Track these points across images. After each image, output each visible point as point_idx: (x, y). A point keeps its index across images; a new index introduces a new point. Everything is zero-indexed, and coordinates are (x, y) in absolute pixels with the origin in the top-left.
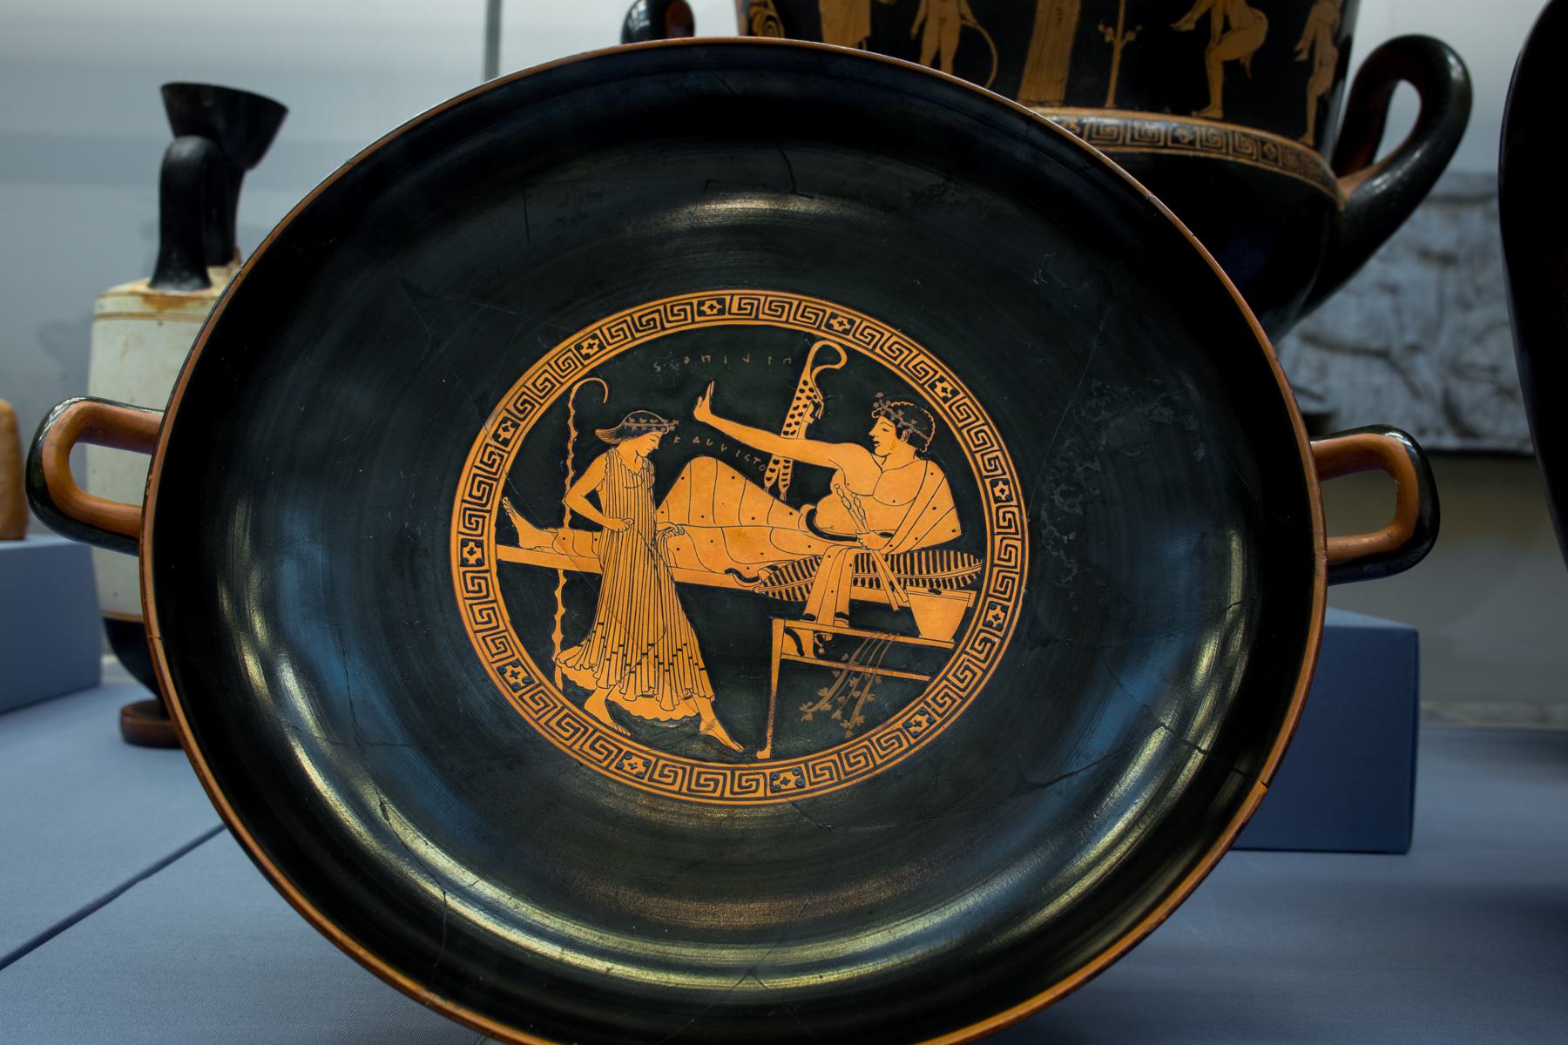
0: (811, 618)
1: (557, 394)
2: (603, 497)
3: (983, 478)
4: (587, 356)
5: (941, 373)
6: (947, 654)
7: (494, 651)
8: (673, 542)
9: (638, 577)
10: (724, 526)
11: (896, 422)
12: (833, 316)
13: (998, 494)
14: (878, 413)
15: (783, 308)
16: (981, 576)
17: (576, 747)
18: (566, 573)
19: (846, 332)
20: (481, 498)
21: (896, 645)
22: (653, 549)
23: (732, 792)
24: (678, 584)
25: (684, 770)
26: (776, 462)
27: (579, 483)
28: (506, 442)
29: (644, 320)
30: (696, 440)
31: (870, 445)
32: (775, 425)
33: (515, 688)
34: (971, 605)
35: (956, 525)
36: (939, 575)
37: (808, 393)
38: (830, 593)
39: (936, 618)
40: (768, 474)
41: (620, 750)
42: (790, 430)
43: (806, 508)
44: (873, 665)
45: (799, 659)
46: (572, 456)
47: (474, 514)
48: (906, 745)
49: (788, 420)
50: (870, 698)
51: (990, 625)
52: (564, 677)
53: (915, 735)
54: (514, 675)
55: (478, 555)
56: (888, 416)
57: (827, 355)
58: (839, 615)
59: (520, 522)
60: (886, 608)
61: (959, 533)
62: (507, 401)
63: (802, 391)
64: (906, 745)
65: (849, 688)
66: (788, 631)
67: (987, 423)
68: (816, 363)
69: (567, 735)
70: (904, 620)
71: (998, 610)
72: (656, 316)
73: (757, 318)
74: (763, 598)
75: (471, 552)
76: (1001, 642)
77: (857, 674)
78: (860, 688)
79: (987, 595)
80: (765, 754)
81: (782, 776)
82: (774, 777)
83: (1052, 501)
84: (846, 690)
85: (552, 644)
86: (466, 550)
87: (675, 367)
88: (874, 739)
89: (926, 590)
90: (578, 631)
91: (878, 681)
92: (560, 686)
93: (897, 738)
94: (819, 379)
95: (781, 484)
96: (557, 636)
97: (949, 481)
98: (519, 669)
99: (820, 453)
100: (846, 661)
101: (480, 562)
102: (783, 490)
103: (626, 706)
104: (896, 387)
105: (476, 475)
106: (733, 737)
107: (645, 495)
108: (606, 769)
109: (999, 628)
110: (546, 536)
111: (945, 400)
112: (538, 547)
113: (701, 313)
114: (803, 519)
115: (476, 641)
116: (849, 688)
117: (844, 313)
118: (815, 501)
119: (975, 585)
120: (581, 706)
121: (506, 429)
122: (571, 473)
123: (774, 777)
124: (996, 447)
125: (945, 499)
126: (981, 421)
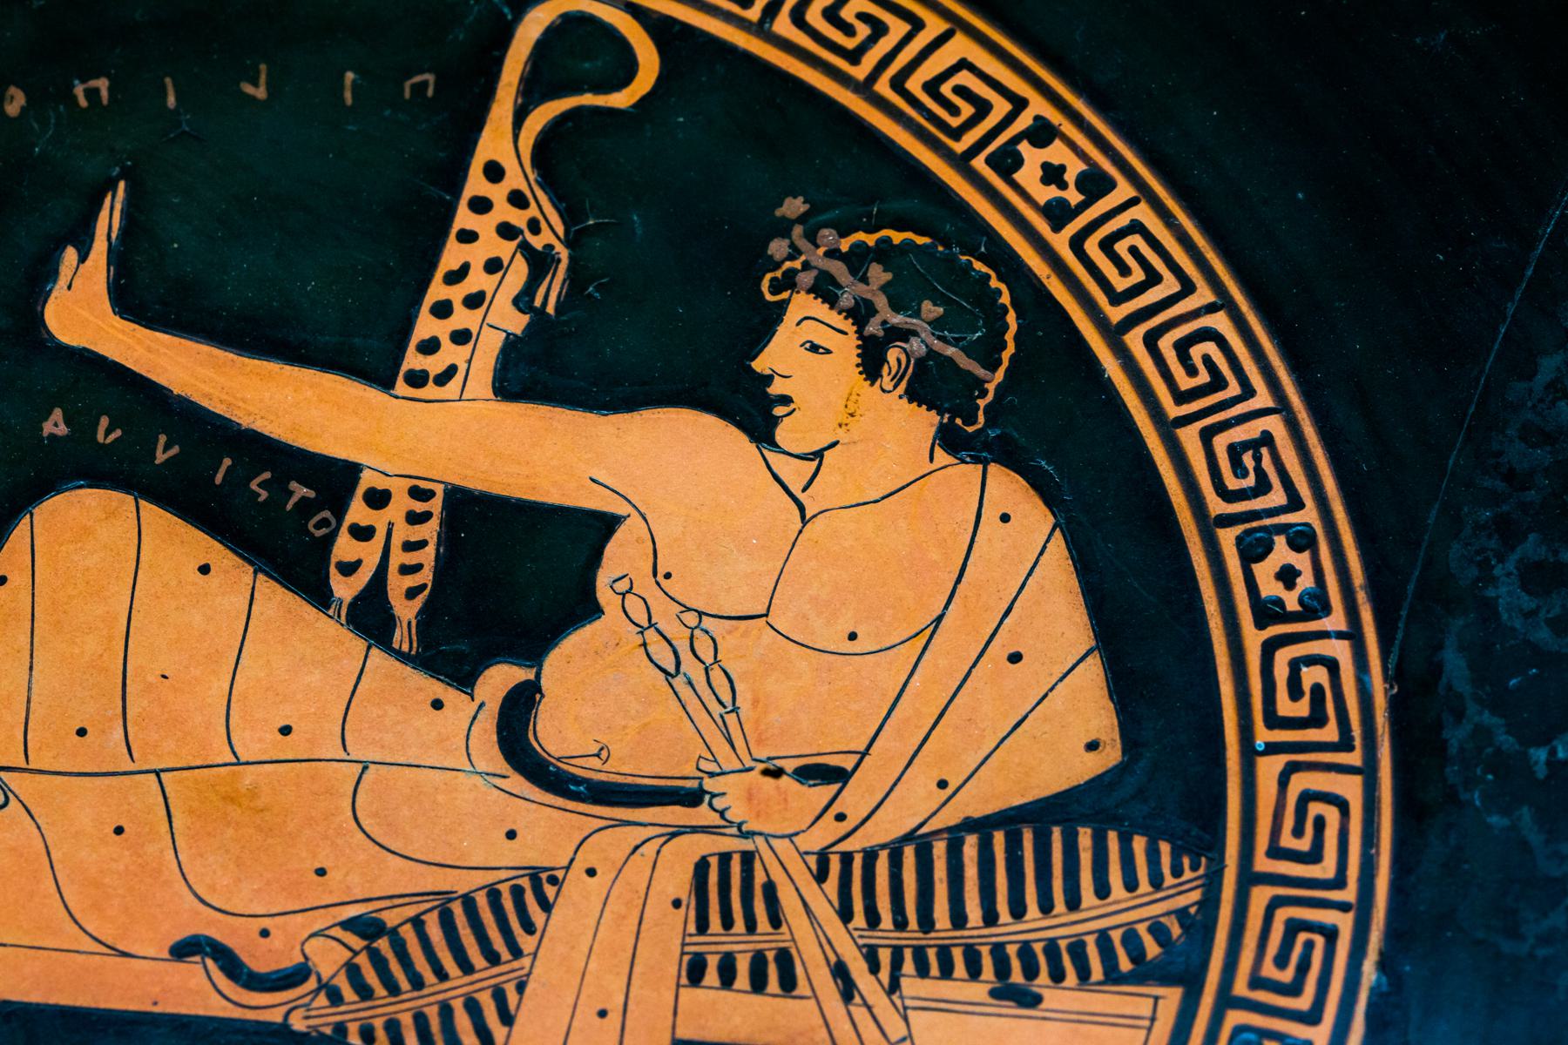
3: (1209, 526)
5: (1038, 106)
11: (860, 313)
13: (1270, 589)
14: (788, 282)
26: (378, 499)
31: (755, 412)
32: (374, 357)
35: (1101, 719)
40: (345, 547)
43: (500, 679)
49: (427, 325)
56: (825, 290)
63: (481, 205)
67: (1224, 303)
68: (533, 91)
79: (1226, 1000)
83: (1488, 609)
95: (397, 585)
97: (1073, 545)
102: (406, 611)
111: (1058, 214)
118: (533, 648)
124: (1263, 399)
125: (1058, 619)
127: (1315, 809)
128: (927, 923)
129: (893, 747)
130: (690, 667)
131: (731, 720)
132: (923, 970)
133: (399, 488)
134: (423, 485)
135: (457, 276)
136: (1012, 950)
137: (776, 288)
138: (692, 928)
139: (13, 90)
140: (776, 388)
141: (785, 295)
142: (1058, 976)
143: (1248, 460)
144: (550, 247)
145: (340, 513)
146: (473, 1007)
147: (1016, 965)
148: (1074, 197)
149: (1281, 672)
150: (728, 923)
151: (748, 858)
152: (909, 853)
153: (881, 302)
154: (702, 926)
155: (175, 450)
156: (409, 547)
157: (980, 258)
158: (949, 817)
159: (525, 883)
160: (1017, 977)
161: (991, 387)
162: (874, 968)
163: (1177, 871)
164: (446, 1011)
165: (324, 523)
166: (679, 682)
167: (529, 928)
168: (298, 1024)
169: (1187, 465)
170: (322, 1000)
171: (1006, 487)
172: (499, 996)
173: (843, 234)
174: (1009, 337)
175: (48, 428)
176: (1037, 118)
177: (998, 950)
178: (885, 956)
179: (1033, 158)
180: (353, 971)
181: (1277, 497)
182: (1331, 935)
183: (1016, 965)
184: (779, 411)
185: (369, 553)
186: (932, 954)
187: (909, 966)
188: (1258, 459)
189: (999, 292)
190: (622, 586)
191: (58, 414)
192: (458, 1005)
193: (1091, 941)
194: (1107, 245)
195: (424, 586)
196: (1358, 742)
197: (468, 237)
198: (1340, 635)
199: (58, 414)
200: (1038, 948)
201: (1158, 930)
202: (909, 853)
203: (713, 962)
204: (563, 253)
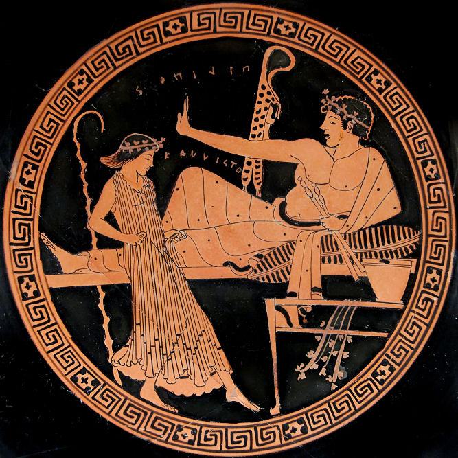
0: (293, 295)
3: (415, 160)
4: (80, 92)
5: (375, 66)
6: (399, 313)
9: (158, 281)
10: (217, 226)
11: (342, 115)
13: (428, 173)
14: (326, 109)
15: (236, 18)
17: (142, 429)
18: (104, 288)
19: (292, 35)
20: (23, 239)
22: (166, 257)
24: (189, 281)
25: (221, 432)
27: (96, 208)
28: (31, 184)
29: (120, 48)
31: (322, 138)
32: (242, 129)
33: (87, 391)
34: (413, 271)
35: (397, 203)
39: (388, 284)
40: (244, 175)
41: (173, 425)
42: (256, 132)
43: (278, 201)
44: (344, 328)
46: (86, 185)
47: (22, 255)
48: (376, 391)
49: (254, 124)
50: (346, 356)
52: (121, 374)
53: (382, 382)
54: (84, 381)
55: (33, 288)
58: (314, 289)
59: (59, 253)
60: (349, 279)
61: (399, 210)
62: (23, 147)
63: (262, 95)
64: (376, 391)
65: (329, 349)
66: (278, 308)
68: (271, 67)
69: (133, 421)
70: (363, 289)
71: (434, 274)
72: (130, 42)
73: (215, 31)
74: (254, 284)
75: (28, 287)
76: (438, 301)
77: (333, 337)
78: (337, 348)
79: (425, 262)
80: (275, 410)
81: (291, 426)
82: (285, 427)
84: (327, 351)
85: (105, 348)
86: (23, 285)
88: (352, 389)
89: (377, 261)
91: (350, 341)
92: (120, 382)
93: (369, 386)
95: (255, 182)
96: (108, 342)
97: (389, 164)
99: (283, 151)
100: (324, 328)
101: (36, 294)
102: (258, 188)
104: (340, 85)
105: (14, 220)
107: (151, 209)
109: (436, 288)
110: (82, 257)
112: (82, 270)
113: (168, 34)
114: (277, 210)
115: (49, 360)
116: (329, 349)
117: (288, 17)
118: (284, 194)
119: (416, 254)
122: (89, 201)
123: (285, 427)
124: (425, 131)
125: (387, 181)
128: (366, 247)
130: (315, 195)
135: (258, 112)
136: (383, 252)
137: (324, 110)
138: (322, 251)
140: (325, 133)
142: (392, 257)
143: (422, 145)
146: (282, 272)
147: (384, 255)
149: (431, 191)
151: (331, 236)
154: (324, 251)
156: (257, 174)
157: (366, 102)
158: (369, 224)
160: (385, 258)
161: (369, 130)
162: (357, 257)
163: (414, 234)
164: (277, 273)
165: (239, 170)
166: (313, 199)
168: (250, 278)
169: (410, 147)
170: (254, 272)
171: (374, 152)
172: (287, 269)
177: (381, 252)
178: (359, 254)
179: (375, 78)
180: (259, 266)
181: (428, 153)
183: (384, 255)
185: (249, 176)
186: (368, 254)
187: (364, 256)
190: (300, 179)
196: (447, 206)
197: (260, 103)
198: (443, 183)
201: (411, 247)
203: (326, 258)
204: (280, 105)
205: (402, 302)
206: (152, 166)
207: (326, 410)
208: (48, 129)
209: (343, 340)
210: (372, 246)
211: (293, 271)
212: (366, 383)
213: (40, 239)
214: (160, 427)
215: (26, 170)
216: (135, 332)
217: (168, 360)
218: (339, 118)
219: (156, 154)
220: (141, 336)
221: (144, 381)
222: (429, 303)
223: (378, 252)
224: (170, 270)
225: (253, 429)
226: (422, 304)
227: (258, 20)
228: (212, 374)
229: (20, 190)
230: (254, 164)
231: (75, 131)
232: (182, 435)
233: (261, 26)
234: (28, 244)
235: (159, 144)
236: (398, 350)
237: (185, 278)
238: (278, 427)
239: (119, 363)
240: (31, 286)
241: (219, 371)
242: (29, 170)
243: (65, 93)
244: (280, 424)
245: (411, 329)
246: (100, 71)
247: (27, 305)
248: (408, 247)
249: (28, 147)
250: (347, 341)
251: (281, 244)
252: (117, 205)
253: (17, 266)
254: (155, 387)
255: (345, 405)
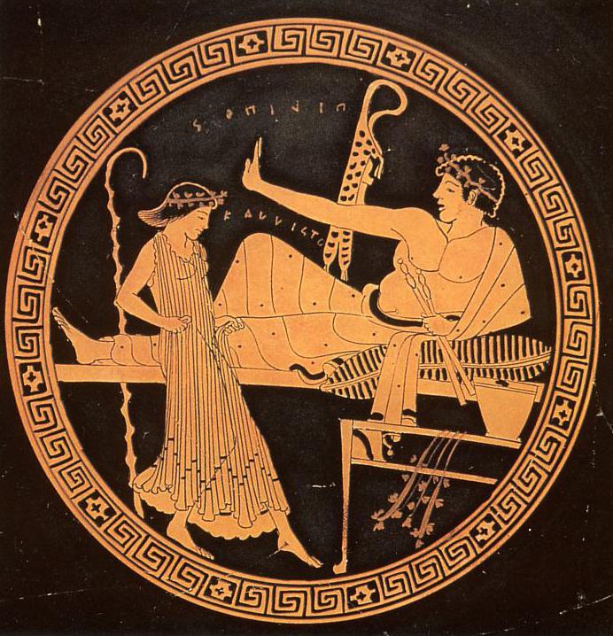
0: (379, 417)
1: (92, 175)
2: (155, 292)
4: (118, 122)
5: (512, 120)
7: (73, 485)
8: (233, 340)
9: (202, 382)
10: (282, 315)
11: (463, 180)
12: (391, 48)
13: (570, 270)
15: (333, 39)
16: (549, 366)
17: (165, 578)
18: (131, 387)
19: (405, 68)
20: (30, 314)
21: (465, 445)
23: (313, 611)
24: (244, 387)
28: (45, 242)
29: (176, 67)
30: (248, 215)
31: (434, 208)
32: (329, 189)
33: (100, 521)
34: (538, 400)
35: (526, 305)
36: (507, 364)
37: (365, 146)
38: (397, 389)
40: (327, 250)
41: (206, 576)
42: (348, 194)
44: (441, 467)
45: (369, 463)
46: (117, 247)
48: (473, 555)
51: (555, 422)
52: (144, 503)
53: (482, 543)
55: (38, 381)
56: (453, 172)
57: (386, 98)
59: (74, 335)
62: (40, 193)
63: (359, 144)
65: (418, 494)
66: (357, 433)
67: (561, 184)
70: (470, 417)
71: (565, 407)
72: (189, 60)
73: (304, 54)
74: (330, 398)
75: (32, 378)
76: (567, 440)
77: (426, 477)
79: (555, 388)
81: (358, 590)
82: (351, 591)
84: (415, 496)
85: (127, 469)
86: (26, 375)
87: (217, 124)
88: (442, 549)
89: (493, 381)
90: (149, 453)
91: (446, 485)
92: (141, 514)
93: (464, 547)
94: (381, 129)
95: (341, 261)
96: (131, 460)
98: (99, 501)
100: (415, 464)
101: (42, 388)
102: (344, 268)
103: (206, 527)
104: (465, 139)
105: (21, 287)
106: (311, 551)
108: (196, 597)
113: (241, 52)
114: (367, 300)
115: (52, 476)
116: (418, 494)
117: (405, 43)
119: (544, 377)
120: (163, 532)
121: (43, 226)
122: (120, 268)
123: (351, 591)
124: (570, 214)
126: (555, 181)
127: (579, 335)
128: (480, 362)
129: (474, 307)
130: (419, 286)
131: (429, 301)
132: (479, 375)
133: (340, 232)
134: (347, 231)
135: (353, 167)
136: (501, 370)
137: (440, 171)
139: (229, 111)
140: (439, 202)
141: (442, 174)
142: (513, 378)
143: (565, 231)
144: (378, 158)
145: (325, 239)
146: (366, 384)
147: (502, 374)
148: (521, 149)
149: (572, 295)
150: (430, 361)
151: (435, 342)
152: (475, 340)
153: (468, 177)
154: (423, 361)
155: (280, 221)
156: (344, 249)
159: (378, 348)
161: (497, 204)
162: (467, 374)
163: (544, 351)
167: (380, 361)
168: (323, 390)
170: (329, 382)
171: (501, 234)
172: (373, 381)
173: (458, 156)
174: (503, 190)
175: (246, 216)
176: (512, 124)
177: (498, 370)
178: (469, 370)
180: (336, 374)
181: (573, 243)
182: (582, 371)
183: (502, 374)
184: (440, 209)
185: (333, 251)
187: (475, 374)
188: (568, 231)
189: (499, 177)
190: (400, 261)
191: (248, 211)
192: (362, 383)
193: (521, 369)
194: (530, 164)
195: (347, 262)
197: (356, 154)
199: (248, 211)
200: (508, 370)
201: (539, 367)
202: (475, 340)
203: (426, 371)
204: (382, 160)
205: (519, 440)
206: (207, 228)
207: (405, 573)
208: (72, 169)
209: (437, 483)
210: (488, 361)
211: (379, 384)
212: (461, 544)
213: (52, 316)
214: (189, 577)
215: (40, 222)
216: (166, 449)
217: (207, 489)
218: (459, 184)
219: (212, 211)
220: (174, 454)
221: (173, 515)
222: (555, 445)
223: (495, 370)
224: (219, 369)
225: (308, 590)
226: (546, 444)
227: (362, 44)
228: (262, 513)
229: (31, 248)
230: (341, 236)
231: (108, 174)
232: (217, 590)
233: (365, 52)
234: (35, 321)
235: (218, 200)
236: (508, 504)
237: (237, 381)
238: (341, 590)
239: (142, 488)
240: (35, 377)
241: (271, 510)
242: (44, 223)
243: (98, 122)
244: (345, 587)
245: (527, 476)
246: (148, 96)
247: (29, 402)
248: (534, 366)
249: (45, 192)
250: (442, 485)
251: (369, 347)
252: (156, 278)
253: (20, 349)
254: (187, 524)
255: (431, 569)
